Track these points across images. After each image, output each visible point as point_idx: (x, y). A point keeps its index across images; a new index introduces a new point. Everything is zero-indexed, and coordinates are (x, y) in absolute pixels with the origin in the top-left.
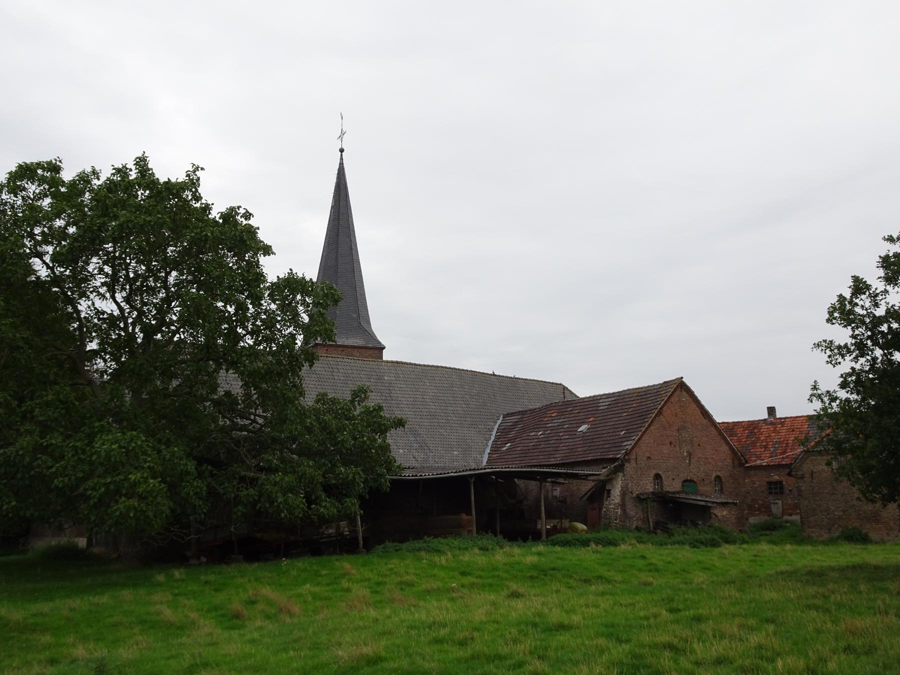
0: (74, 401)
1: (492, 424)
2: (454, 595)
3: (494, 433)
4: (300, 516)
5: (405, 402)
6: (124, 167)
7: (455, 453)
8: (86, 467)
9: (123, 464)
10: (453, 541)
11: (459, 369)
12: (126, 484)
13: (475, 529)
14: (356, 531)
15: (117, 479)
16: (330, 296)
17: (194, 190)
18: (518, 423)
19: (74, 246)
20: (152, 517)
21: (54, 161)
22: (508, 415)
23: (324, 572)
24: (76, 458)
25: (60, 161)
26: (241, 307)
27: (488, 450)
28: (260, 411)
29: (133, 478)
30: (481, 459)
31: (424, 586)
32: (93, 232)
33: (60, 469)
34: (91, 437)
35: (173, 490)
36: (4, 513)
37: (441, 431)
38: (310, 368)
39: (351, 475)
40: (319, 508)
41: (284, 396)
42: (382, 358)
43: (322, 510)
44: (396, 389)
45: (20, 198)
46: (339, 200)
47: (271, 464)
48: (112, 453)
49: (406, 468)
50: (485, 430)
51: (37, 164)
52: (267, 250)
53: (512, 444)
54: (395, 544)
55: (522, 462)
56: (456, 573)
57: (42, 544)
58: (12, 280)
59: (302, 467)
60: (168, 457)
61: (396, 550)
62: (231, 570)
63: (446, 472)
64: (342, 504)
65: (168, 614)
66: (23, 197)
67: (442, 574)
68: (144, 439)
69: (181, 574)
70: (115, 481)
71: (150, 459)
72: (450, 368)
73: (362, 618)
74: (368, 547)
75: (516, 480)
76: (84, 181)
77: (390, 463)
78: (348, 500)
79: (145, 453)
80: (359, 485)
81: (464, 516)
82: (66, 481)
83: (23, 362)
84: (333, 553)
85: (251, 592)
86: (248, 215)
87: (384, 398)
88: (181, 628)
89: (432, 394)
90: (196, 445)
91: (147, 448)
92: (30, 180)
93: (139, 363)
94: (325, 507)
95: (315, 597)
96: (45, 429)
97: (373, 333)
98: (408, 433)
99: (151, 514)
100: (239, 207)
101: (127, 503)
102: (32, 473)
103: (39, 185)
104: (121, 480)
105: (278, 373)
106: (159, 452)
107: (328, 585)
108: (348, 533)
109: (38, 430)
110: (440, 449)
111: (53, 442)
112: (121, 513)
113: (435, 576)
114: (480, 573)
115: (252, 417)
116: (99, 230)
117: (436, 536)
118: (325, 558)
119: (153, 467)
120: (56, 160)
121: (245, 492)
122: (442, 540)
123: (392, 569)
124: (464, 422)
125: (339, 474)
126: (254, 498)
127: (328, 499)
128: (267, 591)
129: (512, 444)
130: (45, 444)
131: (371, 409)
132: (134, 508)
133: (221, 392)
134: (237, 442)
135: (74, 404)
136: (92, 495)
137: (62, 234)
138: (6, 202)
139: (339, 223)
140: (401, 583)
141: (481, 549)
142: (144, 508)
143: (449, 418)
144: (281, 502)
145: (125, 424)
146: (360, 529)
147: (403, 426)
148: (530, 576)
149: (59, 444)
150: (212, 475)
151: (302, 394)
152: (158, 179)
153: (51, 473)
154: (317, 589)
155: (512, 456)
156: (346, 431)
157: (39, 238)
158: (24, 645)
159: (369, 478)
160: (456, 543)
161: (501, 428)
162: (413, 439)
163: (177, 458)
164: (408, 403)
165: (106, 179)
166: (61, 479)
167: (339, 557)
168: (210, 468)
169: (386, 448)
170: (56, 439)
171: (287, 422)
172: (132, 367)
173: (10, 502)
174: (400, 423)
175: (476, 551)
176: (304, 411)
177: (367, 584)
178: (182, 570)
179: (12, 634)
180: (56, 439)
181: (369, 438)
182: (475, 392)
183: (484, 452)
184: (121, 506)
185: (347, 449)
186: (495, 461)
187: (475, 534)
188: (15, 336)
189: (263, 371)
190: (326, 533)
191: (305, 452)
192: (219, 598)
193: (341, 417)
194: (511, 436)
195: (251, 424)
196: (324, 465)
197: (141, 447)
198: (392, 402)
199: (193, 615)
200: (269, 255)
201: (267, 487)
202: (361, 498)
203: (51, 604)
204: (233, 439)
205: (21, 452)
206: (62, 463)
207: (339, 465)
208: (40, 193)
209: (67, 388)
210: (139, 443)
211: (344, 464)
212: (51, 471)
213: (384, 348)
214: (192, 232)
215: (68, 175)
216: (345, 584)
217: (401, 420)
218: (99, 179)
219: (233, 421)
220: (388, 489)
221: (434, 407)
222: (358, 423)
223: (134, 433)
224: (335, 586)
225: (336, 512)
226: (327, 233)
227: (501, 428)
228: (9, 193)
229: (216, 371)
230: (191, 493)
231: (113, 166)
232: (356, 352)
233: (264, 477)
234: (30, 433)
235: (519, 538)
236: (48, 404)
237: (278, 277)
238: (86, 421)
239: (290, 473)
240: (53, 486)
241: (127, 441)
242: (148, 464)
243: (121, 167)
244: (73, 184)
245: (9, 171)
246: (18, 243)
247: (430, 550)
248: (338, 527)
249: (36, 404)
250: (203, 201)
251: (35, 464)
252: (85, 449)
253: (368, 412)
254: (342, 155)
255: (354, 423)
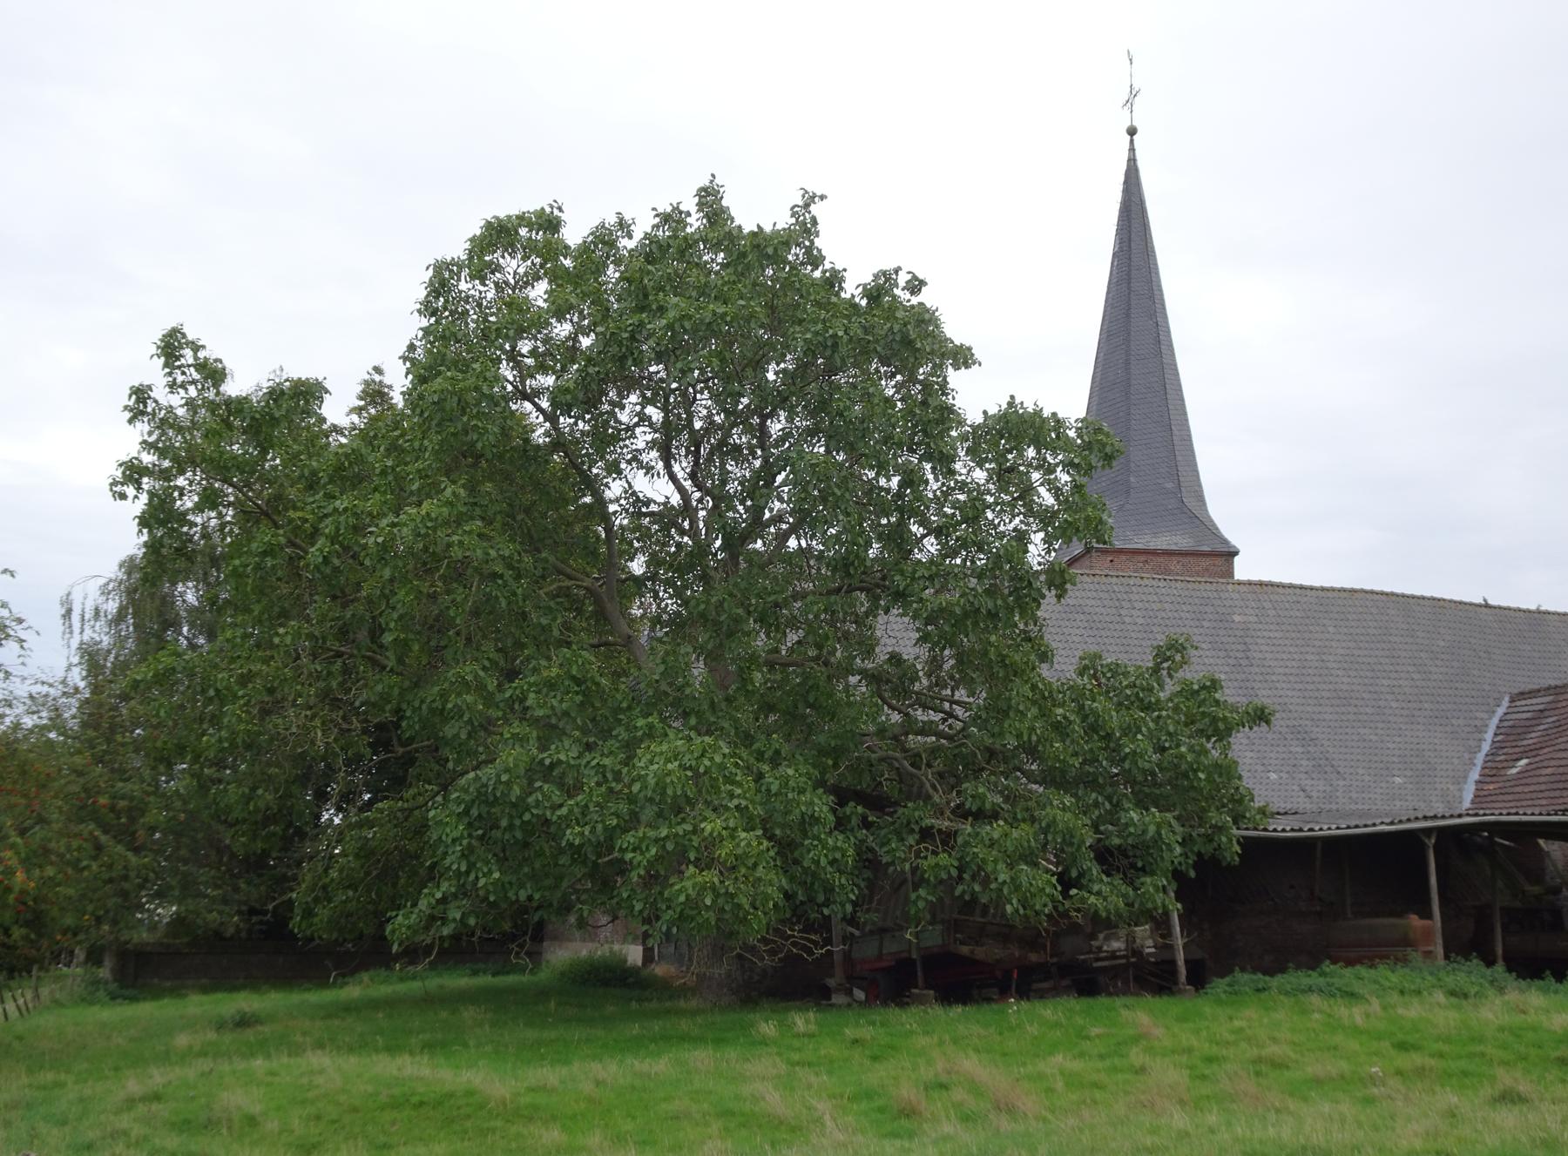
0: (598, 679)
1: (1485, 716)
2: (1375, 1090)
3: (1489, 736)
4: (1046, 911)
5: (1281, 670)
6: (676, 209)
7: (1398, 780)
8: (624, 808)
9: (689, 801)
10: (1389, 973)
11: (1403, 596)
12: (696, 841)
13: (1440, 951)
14: (1170, 948)
15: (680, 830)
16: (1096, 448)
17: (807, 243)
18: (1547, 713)
19: (588, 374)
20: (747, 907)
21: (548, 210)
22: (1522, 695)
23: (1095, 1031)
24: (603, 789)
25: (560, 209)
26: (912, 480)
27: (1475, 775)
28: (961, 694)
29: (709, 828)
30: (1457, 794)
31: (1309, 1069)
32: (620, 344)
33: (576, 810)
34: (630, 747)
35: (787, 851)
36: (481, 893)
37: (1362, 731)
38: (1059, 601)
39: (1152, 829)
40: (1086, 895)
41: (1003, 661)
42: (1230, 573)
43: (1092, 899)
44: (1259, 641)
45: (492, 285)
46: (1130, 240)
47: (984, 803)
48: (668, 780)
49: (1278, 813)
50: (1469, 729)
51: (518, 217)
52: (963, 357)
53: (1532, 760)
54: (1254, 977)
55: (1556, 801)
56: (1386, 1044)
57: (563, 954)
58: (479, 445)
59: (1048, 809)
60: (774, 788)
61: (1258, 990)
62: (907, 1019)
63: (1369, 822)
64: (1136, 889)
65: (774, 1100)
66: (496, 284)
67: (1353, 1045)
68: (727, 751)
69: (807, 1022)
70: (676, 835)
71: (739, 791)
72: (1382, 593)
73: (1154, 1131)
74: (1199, 978)
75: (1541, 842)
76: (604, 243)
77: (1240, 802)
78: (1148, 880)
79: (730, 780)
80: (1171, 850)
81: (1415, 921)
82: (587, 833)
83: (504, 603)
84: (1125, 992)
85: (940, 1066)
86: (916, 285)
87: (1231, 661)
88: (793, 1130)
89: (1342, 652)
90: (830, 762)
91: (734, 770)
92: (507, 250)
93: (714, 600)
94: (1099, 893)
95: (1073, 1081)
96: (549, 731)
97: (1212, 521)
98: (1289, 736)
99: (744, 901)
100: (897, 271)
101: (700, 879)
102: (527, 817)
103: (525, 259)
104: (686, 833)
105: (989, 611)
106: (760, 777)
107: (1101, 1057)
108: (1153, 950)
109: (535, 734)
110: (1361, 771)
111: (563, 757)
112: (688, 896)
113: (1335, 1048)
114: (1440, 1046)
115: (947, 705)
116: (633, 338)
117: (1350, 963)
118: (1103, 1001)
119: (747, 807)
120: (552, 207)
121: (932, 860)
122: (1362, 971)
123: (1241, 1029)
124: (1417, 713)
125: (1127, 825)
126: (949, 872)
127: (1104, 878)
128: (970, 1064)
129: (1532, 760)
130: (547, 762)
131: (1196, 687)
132: (713, 888)
133: (882, 654)
134: (915, 758)
135: (598, 684)
136: (635, 862)
137: (570, 349)
138: (468, 297)
139: (1129, 288)
140: (1259, 1060)
141: (1453, 993)
142: (731, 890)
143: (1382, 703)
144: (1005, 882)
145: (693, 721)
146: (1179, 941)
147: (1268, 722)
148: (1558, 1059)
149: (572, 762)
150: (866, 824)
151: (1045, 657)
152: (740, 227)
153: (559, 817)
154: (1076, 1065)
155: (1532, 788)
156: (1140, 732)
157: (530, 361)
158: (514, 1145)
159: (1194, 834)
160: (1394, 978)
161: (1506, 724)
162: (1300, 749)
163: (793, 790)
164: (1287, 670)
165: (642, 236)
166: (577, 829)
167: (1130, 1000)
168: (860, 809)
169: (1227, 771)
170: (565, 752)
171: (1012, 714)
172: (703, 606)
173: (490, 872)
174: (1261, 716)
175: (1440, 997)
176: (1050, 692)
177: (1184, 1059)
178: (811, 1015)
179: (492, 1124)
180: (565, 752)
181: (1191, 749)
182: (1442, 644)
183: (1466, 777)
184: (688, 884)
185: (1144, 771)
186: (1493, 798)
187: (1441, 962)
188: (488, 554)
189: (958, 611)
190: (1105, 948)
191: (1056, 779)
192: (877, 1075)
193: (1132, 703)
194: (1531, 742)
195: (944, 720)
196: (1096, 804)
197: (722, 767)
198: (1252, 669)
199: (823, 1106)
200: (967, 366)
201: (975, 850)
202: (1177, 875)
203: (564, 1071)
204: (905, 750)
205: (504, 778)
206: (580, 798)
207: (1127, 805)
208: (526, 274)
209: (583, 653)
210: (718, 759)
211: (1142, 804)
212: (558, 813)
213: (1236, 553)
214: (808, 330)
215: (574, 234)
216: (1136, 1056)
217: (1262, 710)
218: (630, 237)
219: (907, 715)
220: (1237, 858)
221: (1345, 680)
222: (1169, 717)
223: (707, 739)
224: (1116, 1061)
225: (1121, 905)
226: (1105, 311)
227: (1506, 724)
228: (472, 277)
229: (872, 612)
230: (823, 862)
231: (654, 209)
232: (1174, 564)
233: (969, 829)
234: (520, 739)
235: (1548, 972)
236: (551, 685)
237: (985, 412)
238: (622, 717)
239: (1024, 820)
240: (564, 844)
241: (696, 755)
242: (736, 802)
243: (669, 209)
244: (585, 249)
245: (471, 236)
246: (488, 374)
247: (1328, 993)
248: (1131, 939)
249: (529, 683)
250: (828, 266)
251: (530, 800)
252: (620, 772)
253: (1188, 692)
254: (1132, 142)
255: (1159, 717)
